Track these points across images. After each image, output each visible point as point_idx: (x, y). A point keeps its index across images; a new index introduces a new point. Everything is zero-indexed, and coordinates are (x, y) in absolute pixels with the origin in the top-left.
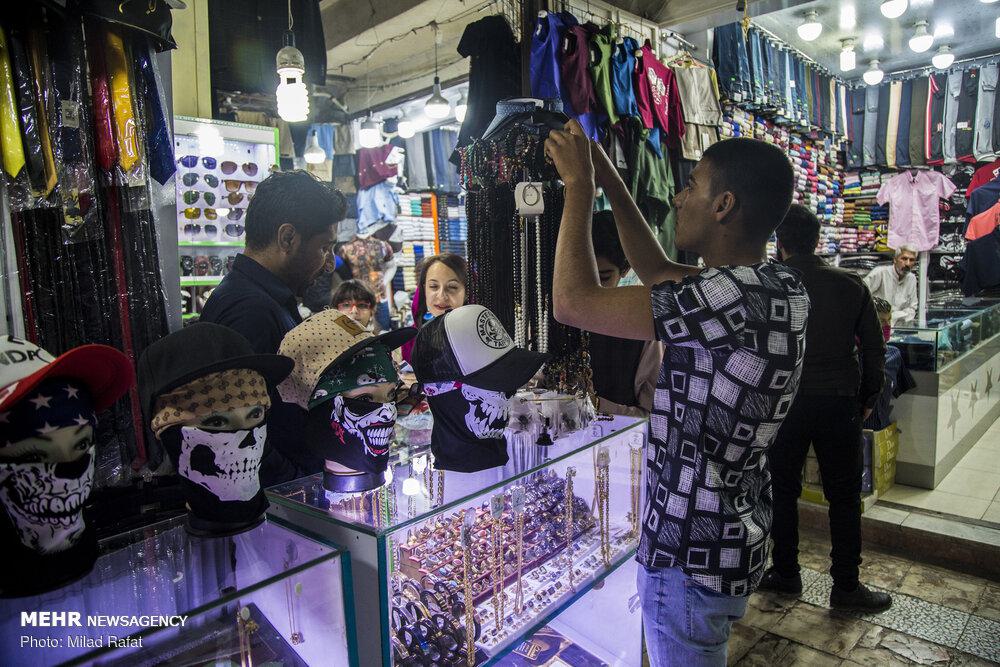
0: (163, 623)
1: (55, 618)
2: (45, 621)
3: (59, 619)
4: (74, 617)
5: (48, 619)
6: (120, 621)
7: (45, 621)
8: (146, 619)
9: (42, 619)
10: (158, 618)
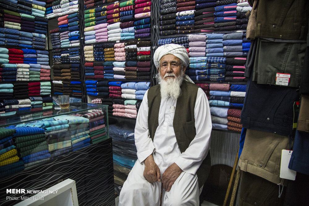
2: (14, 192)
3: (18, 191)
4: (23, 190)
5: (15, 191)
6: (37, 192)
7: (14, 192)
9: (13, 191)
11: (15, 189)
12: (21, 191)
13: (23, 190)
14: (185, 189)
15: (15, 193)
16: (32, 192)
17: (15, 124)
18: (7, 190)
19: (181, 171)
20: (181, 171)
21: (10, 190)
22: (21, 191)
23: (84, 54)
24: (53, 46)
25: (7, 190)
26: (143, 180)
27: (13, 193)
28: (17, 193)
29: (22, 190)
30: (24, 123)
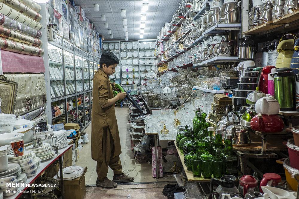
0: (49, 186)
2: (14, 185)
4: (22, 184)
5: (14, 185)
6: (36, 185)
7: (14, 185)
9: (13, 185)
10: (47, 185)
11: (15, 183)
12: (20, 184)
13: (22, 184)
16: (31, 186)
22: (20, 184)
27: (13, 186)
29: (21, 183)
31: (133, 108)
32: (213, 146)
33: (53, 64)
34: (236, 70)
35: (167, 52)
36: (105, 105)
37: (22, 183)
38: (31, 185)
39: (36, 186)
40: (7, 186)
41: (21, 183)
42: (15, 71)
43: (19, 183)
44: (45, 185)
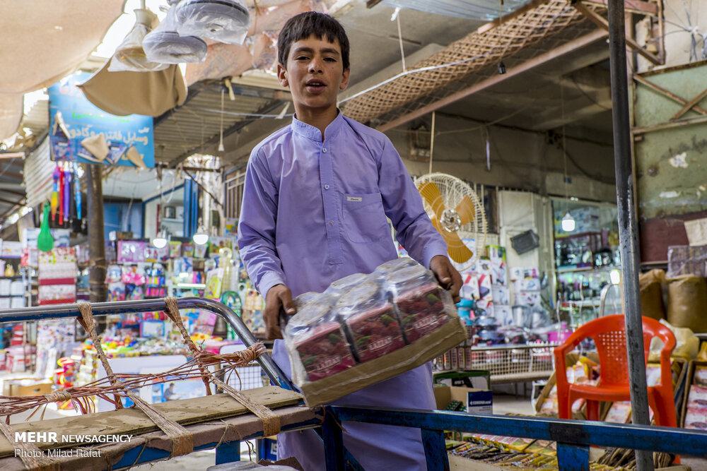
1: (39, 437)
2: (32, 439)
4: (52, 435)
5: (34, 437)
6: (91, 438)
7: (32, 439)
8: (103, 437)
9: (30, 437)
10: (112, 437)
11: (34, 433)
14: (447, 10)
15: (34, 441)
17: (226, 208)
18: (17, 434)
19: (20, 163)
20: (20, 163)
21: (24, 434)
23: (47, 444)
24: (124, 345)
25: (17, 434)
26: (116, 47)
27: (30, 441)
28: (39, 441)
29: (50, 434)
30: (149, 353)
31: (250, 251)
32: (669, 361)
33: (343, 7)
34: (218, 158)
35: (294, 33)
36: (127, 218)
37: (52, 433)
38: (109, 437)
39: (84, 441)
40: (17, 441)
41: (50, 434)
42: (695, 70)
43: (45, 433)
44: (106, 438)
